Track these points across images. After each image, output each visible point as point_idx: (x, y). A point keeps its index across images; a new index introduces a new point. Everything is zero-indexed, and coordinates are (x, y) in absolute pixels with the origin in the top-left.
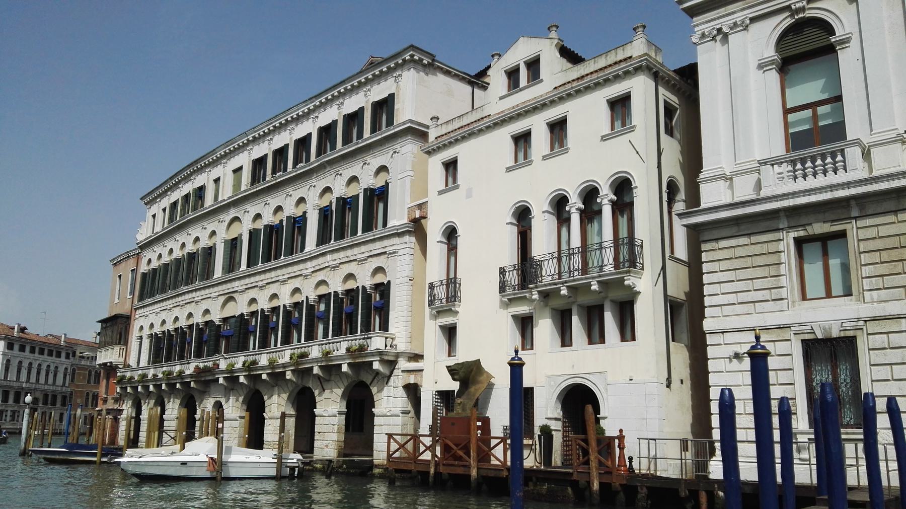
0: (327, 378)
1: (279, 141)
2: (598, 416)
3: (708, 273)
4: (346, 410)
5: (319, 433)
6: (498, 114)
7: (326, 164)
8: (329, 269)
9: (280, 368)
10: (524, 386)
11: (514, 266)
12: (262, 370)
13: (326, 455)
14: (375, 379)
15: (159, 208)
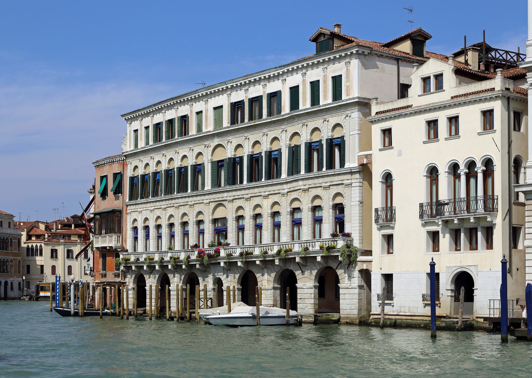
0: (305, 264)
1: (255, 91)
2: (473, 288)
3: (528, 216)
4: (318, 285)
5: (301, 299)
6: (418, 107)
7: (294, 116)
8: (301, 191)
9: (270, 257)
10: (436, 272)
11: (428, 203)
12: (256, 258)
13: (307, 313)
14: (339, 266)
15: (141, 125)
